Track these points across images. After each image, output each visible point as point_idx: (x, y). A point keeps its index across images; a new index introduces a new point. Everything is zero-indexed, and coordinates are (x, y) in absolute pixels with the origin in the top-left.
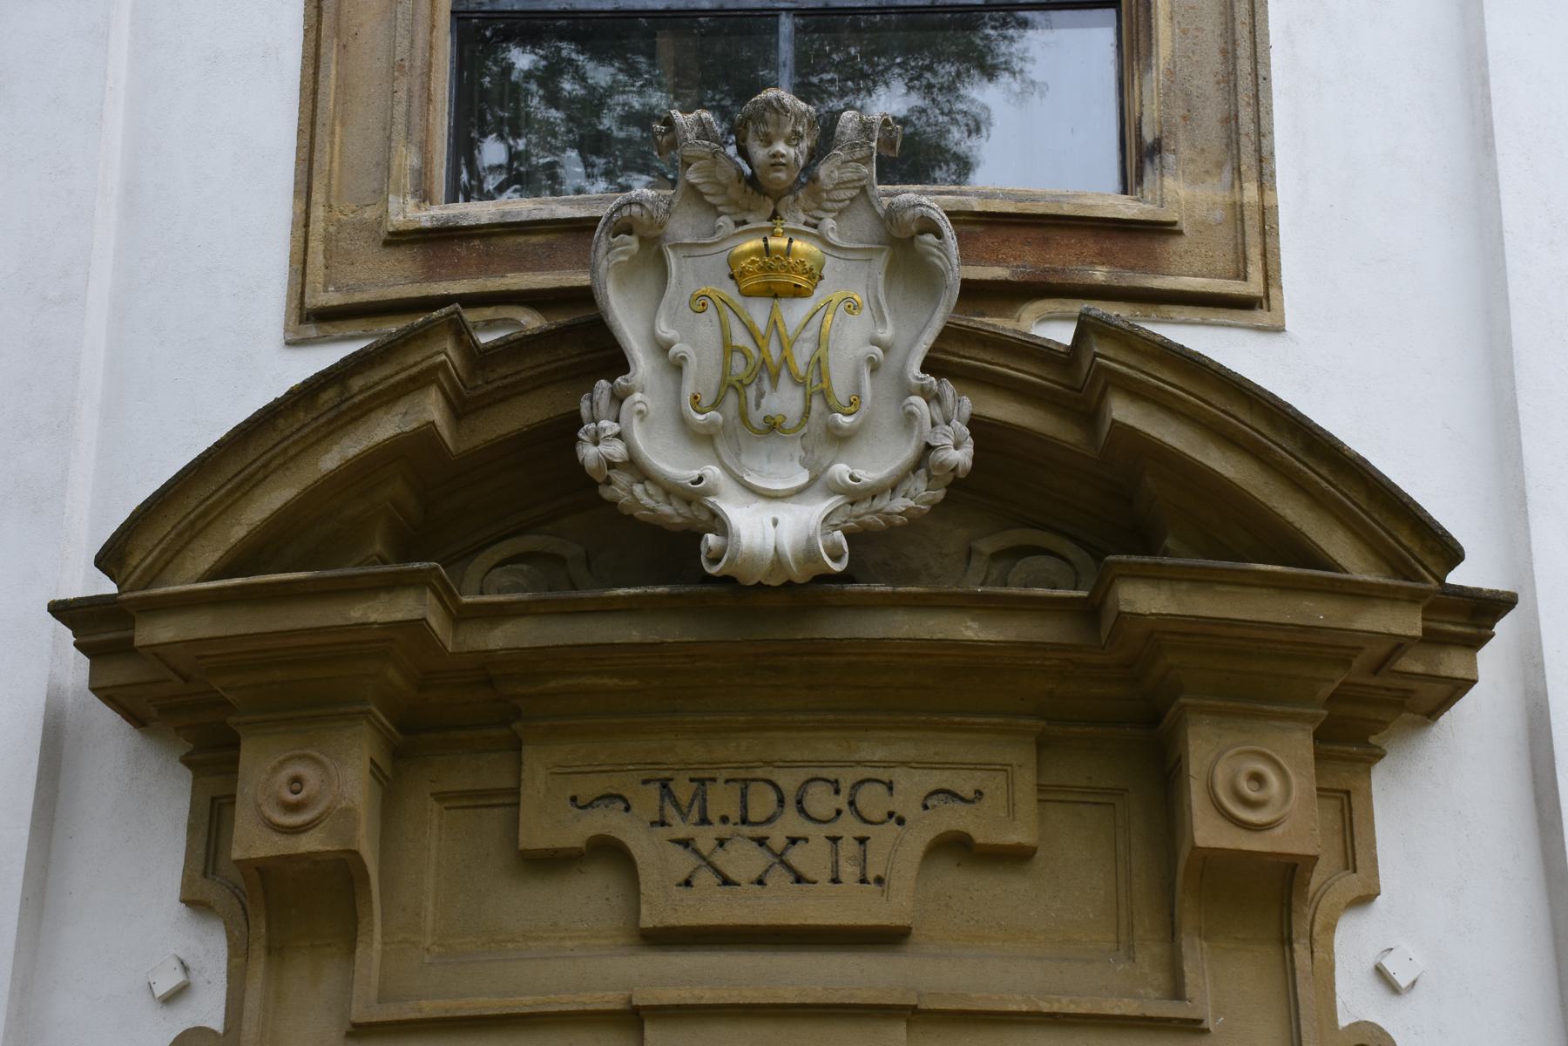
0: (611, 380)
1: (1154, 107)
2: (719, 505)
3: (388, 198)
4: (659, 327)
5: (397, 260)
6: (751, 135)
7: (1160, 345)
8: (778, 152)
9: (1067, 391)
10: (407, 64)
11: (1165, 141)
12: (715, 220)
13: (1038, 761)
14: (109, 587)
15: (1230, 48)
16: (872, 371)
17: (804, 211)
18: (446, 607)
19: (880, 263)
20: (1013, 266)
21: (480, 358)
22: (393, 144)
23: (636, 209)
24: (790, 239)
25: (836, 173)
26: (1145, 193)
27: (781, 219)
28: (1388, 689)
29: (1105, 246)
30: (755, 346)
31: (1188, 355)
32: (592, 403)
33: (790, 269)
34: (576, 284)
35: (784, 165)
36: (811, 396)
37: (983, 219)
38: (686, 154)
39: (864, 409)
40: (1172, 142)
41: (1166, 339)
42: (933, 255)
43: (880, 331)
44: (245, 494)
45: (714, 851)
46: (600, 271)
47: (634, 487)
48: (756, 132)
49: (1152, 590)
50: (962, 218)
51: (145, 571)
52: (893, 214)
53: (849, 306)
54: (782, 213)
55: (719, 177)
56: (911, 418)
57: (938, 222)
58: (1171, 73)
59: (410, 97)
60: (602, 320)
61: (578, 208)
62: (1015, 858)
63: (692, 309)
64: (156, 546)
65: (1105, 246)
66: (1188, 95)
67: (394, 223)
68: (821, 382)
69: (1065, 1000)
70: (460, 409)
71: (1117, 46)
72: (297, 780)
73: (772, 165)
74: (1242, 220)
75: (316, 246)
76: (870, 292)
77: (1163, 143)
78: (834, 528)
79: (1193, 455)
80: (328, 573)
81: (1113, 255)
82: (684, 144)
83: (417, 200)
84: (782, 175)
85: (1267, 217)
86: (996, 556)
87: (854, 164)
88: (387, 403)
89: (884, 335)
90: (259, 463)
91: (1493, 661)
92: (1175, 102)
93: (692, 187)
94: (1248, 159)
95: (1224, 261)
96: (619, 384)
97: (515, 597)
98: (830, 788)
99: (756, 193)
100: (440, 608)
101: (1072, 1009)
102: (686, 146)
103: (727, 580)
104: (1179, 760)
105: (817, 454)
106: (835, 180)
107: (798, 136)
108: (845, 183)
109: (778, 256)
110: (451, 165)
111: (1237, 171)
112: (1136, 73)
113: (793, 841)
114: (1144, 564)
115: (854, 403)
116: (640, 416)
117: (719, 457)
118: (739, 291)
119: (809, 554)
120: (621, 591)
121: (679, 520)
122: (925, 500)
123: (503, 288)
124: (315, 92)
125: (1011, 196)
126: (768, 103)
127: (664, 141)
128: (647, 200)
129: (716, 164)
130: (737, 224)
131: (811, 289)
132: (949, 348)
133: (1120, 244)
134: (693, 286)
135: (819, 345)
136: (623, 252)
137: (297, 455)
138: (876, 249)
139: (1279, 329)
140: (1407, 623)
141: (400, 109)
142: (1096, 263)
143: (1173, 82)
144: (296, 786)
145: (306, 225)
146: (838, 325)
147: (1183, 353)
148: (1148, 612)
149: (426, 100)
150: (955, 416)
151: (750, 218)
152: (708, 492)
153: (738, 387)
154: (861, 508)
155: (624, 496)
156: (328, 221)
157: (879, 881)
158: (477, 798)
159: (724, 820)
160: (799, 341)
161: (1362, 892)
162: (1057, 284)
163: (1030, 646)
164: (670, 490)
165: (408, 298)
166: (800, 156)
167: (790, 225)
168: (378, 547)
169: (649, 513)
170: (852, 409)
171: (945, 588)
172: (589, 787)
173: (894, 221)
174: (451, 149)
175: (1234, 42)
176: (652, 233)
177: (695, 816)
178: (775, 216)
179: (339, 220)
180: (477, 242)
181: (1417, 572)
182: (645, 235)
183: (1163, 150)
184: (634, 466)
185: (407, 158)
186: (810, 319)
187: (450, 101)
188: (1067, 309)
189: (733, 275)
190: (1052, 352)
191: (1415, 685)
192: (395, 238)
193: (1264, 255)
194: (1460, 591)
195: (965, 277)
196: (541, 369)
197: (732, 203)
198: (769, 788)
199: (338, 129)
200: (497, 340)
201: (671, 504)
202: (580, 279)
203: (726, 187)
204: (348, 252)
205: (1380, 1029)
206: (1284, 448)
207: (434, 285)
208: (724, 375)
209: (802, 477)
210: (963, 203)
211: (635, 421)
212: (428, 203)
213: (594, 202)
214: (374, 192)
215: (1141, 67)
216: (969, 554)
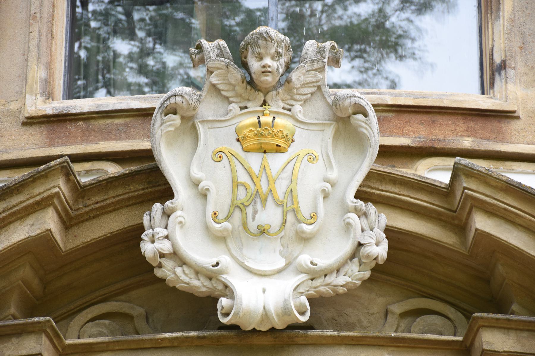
0: (163, 204)
1: (501, 41)
2: (229, 280)
3: (25, 96)
4: (193, 170)
5: (30, 134)
6: (250, 54)
7: (506, 182)
8: (266, 64)
9: (447, 212)
10: (38, 15)
12: (228, 106)
16: (324, 198)
17: (283, 100)
18: (55, 347)
19: (330, 132)
20: (412, 137)
22: (29, 64)
23: (179, 99)
24: (274, 117)
26: (495, 93)
27: (268, 105)
29: (470, 125)
30: (252, 182)
31: (524, 188)
32: (150, 217)
34: (142, 148)
35: (270, 72)
36: (286, 213)
37: (394, 109)
38: (210, 66)
39: (319, 220)
40: (513, 63)
41: (509, 178)
42: (362, 127)
43: (329, 173)
46: (157, 136)
47: (176, 269)
48: (253, 52)
49: (504, 336)
50: (380, 108)
52: (337, 102)
53: (310, 158)
54: (269, 101)
55: (230, 80)
56: (349, 226)
57: (365, 107)
59: (40, 35)
60: (158, 167)
61: (145, 103)
63: (213, 160)
65: (470, 125)
67: (29, 111)
68: (293, 204)
71: (478, 7)
73: (263, 72)
76: (323, 150)
77: (507, 63)
78: (301, 295)
79: (529, 251)
81: (475, 131)
82: (208, 60)
83: (44, 98)
84: (269, 78)
86: (403, 315)
87: (313, 72)
89: (332, 176)
92: (514, 38)
93: (214, 86)
96: (168, 205)
99: (253, 90)
100: (51, 347)
102: (210, 61)
103: (234, 327)
106: (301, 82)
107: (279, 55)
108: (308, 83)
109: (266, 127)
110: (66, 78)
112: (490, 21)
114: (498, 319)
115: (314, 216)
116: (180, 225)
117: (229, 250)
118: (242, 148)
119: (286, 311)
120: (167, 335)
121: (204, 289)
122: (358, 277)
123: (97, 151)
125: (411, 95)
126: (261, 35)
127: (196, 58)
128: (186, 93)
129: (228, 72)
130: (241, 108)
131: (287, 147)
132: (372, 185)
133: (480, 125)
134: (214, 146)
135: (292, 181)
138: (327, 124)
141: (34, 43)
142: (465, 136)
143: (513, 26)
146: (303, 170)
147: (521, 187)
148: (502, 350)
149: (50, 38)
150: (376, 225)
151: (249, 104)
152: (221, 272)
153: (241, 207)
154: (317, 282)
155: (170, 275)
160: (279, 179)
162: (440, 148)
164: (198, 272)
165: (37, 157)
166: (280, 67)
167: (273, 109)
168: (13, 310)
169: (185, 285)
170: (312, 221)
171: (371, 334)
173: (338, 107)
174: (67, 69)
176: (188, 114)
178: (264, 103)
180: (81, 123)
182: (185, 115)
183: (507, 67)
186: (286, 165)
187: (66, 40)
188: (447, 164)
189: (238, 139)
190: (437, 187)
192: (29, 121)
195: (382, 144)
196: (119, 198)
200: (92, 180)
201: (199, 280)
202: (143, 145)
203: (234, 86)
207: (53, 149)
208: (233, 200)
209: (281, 263)
210: (381, 99)
211: (178, 227)
212: (51, 99)
213: (155, 98)
214: (17, 93)
215: (493, 17)
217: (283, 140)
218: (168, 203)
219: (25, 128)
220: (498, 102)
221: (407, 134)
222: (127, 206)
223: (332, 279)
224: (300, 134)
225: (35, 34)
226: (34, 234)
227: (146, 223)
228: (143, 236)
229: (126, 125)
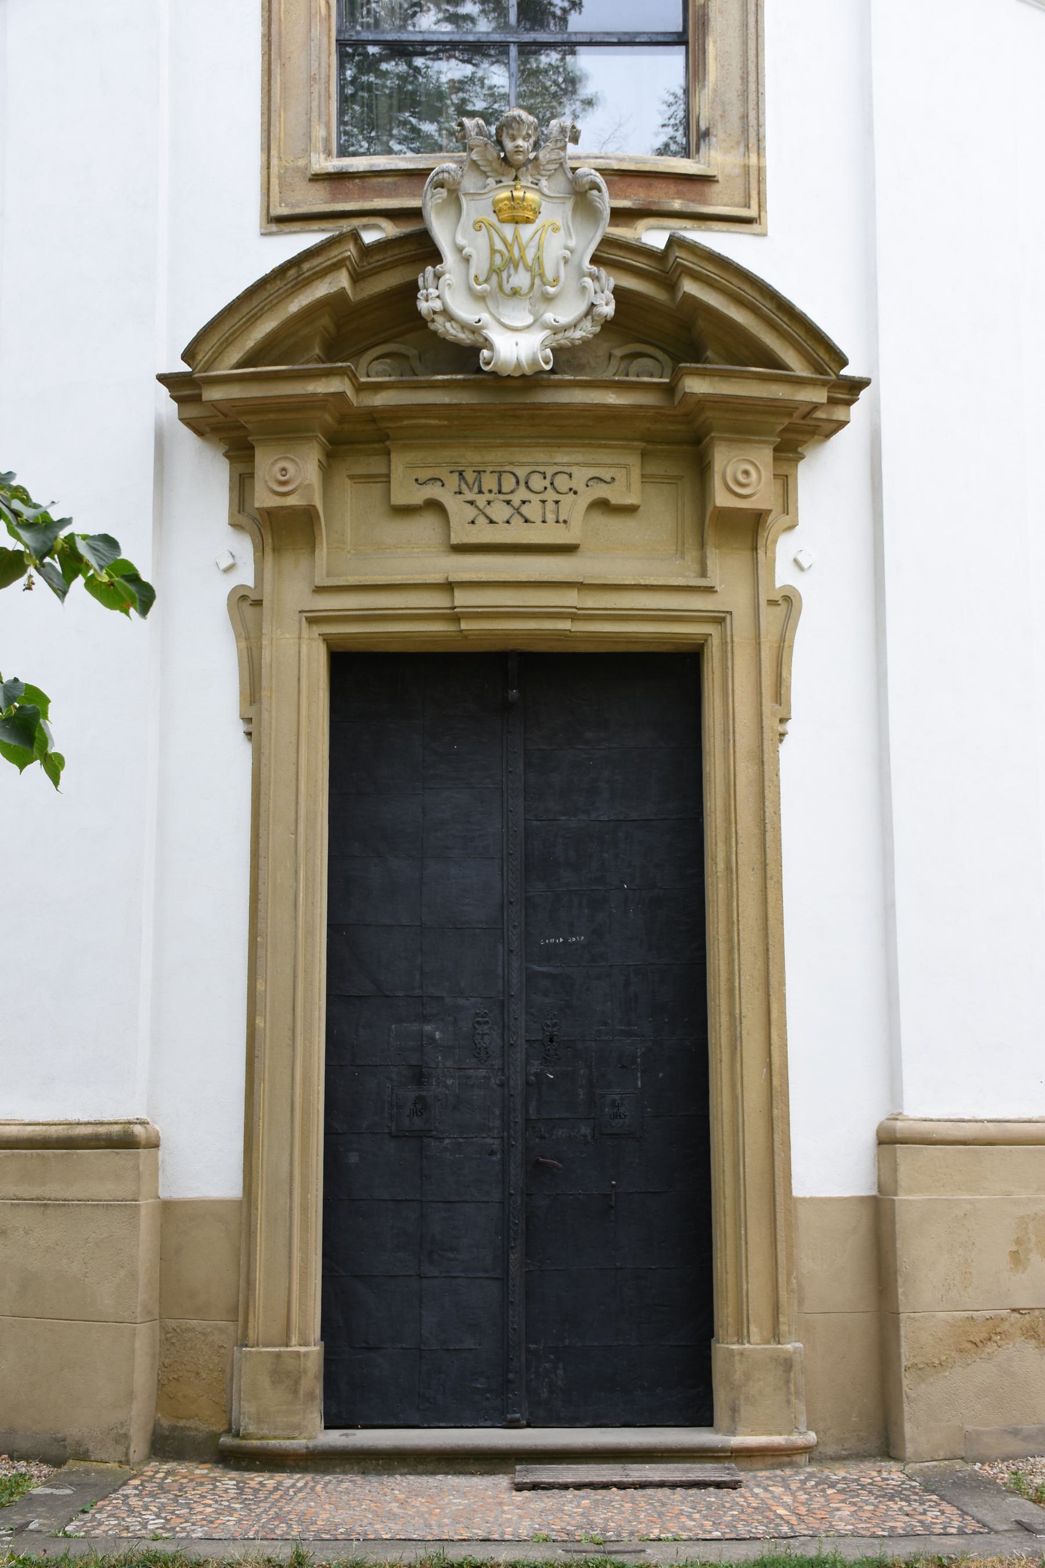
0: (434, 267)
10: (317, 77)
11: (711, 130)
13: (642, 463)
14: (185, 368)
15: (745, 76)
19: (569, 205)
21: (366, 251)
23: (446, 175)
25: (548, 156)
28: (808, 425)
33: (524, 208)
34: (410, 206)
39: (561, 284)
44: (252, 324)
45: (485, 507)
51: (206, 362)
54: (520, 176)
58: (715, 91)
59: (320, 96)
62: (630, 510)
64: (210, 350)
66: (723, 103)
69: (652, 578)
70: (356, 278)
72: (284, 469)
74: (749, 174)
75: (274, 181)
80: (296, 367)
84: (521, 157)
85: (760, 170)
88: (321, 277)
90: (258, 308)
91: (857, 411)
93: (474, 162)
94: (753, 141)
95: (739, 198)
97: (387, 379)
98: (542, 476)
101: (655, 583)
103: (493, 373)
104: (710, 462)
105: (537, 307)
107: (529, 136)
111: (747, 147)
113: (524, 502)
114: (697, 368)
115: (556, 280)
117: (488, 308)
119: (534, 362)
120: (440, 377)
121: (468, 341)
123: (372, 208)
124: (269, 91)
134: (475, 217)
136: (439, 198)
137: (277, 303)
139: (765, 235)
140: (819, 396)
141: (315, 104)
144: (284, 473)
145: (269, 168)
151: (503, 179)
152: (482, 328)
154: (559, 336)
156: (280, 166)
157: (565, 522)
158: (369, 478)
159: (490, 491)
161: (790, 524)
163: (641, 406)
164: (464, 326)
167: (523, 183)
168: (317, 351)
172: (424, 474)
175: (747, 73)
176: (453, 187)
177: (476, 489)
178: (516, 178)
179: (285, 166)
180: (357, 181)
181: (826, 371)
184: (446, 313)
185: (319, 132)
191: (821, 424)
193: (759, 194)
194: (846, 378)
197: (494, 170)
198: (512, 476)
199: (282, 113)
203: (491, 162)
204: (291, 184)
205: (794, 588)
206: (767, 307)
209: (530, 320)
210: (608, 164)
216: (610, 356)
217: (531, 213)
218: (438, 267)
219: (311, 184)
220: (702, 166)
221: (629, 196)
222: (403, 264)
223: (571, 334)
224: (546, 207)
225: (316, 95)
226: (332, 291)
227: (420, 283)
228: (419, 296)
229: (395, 184)
